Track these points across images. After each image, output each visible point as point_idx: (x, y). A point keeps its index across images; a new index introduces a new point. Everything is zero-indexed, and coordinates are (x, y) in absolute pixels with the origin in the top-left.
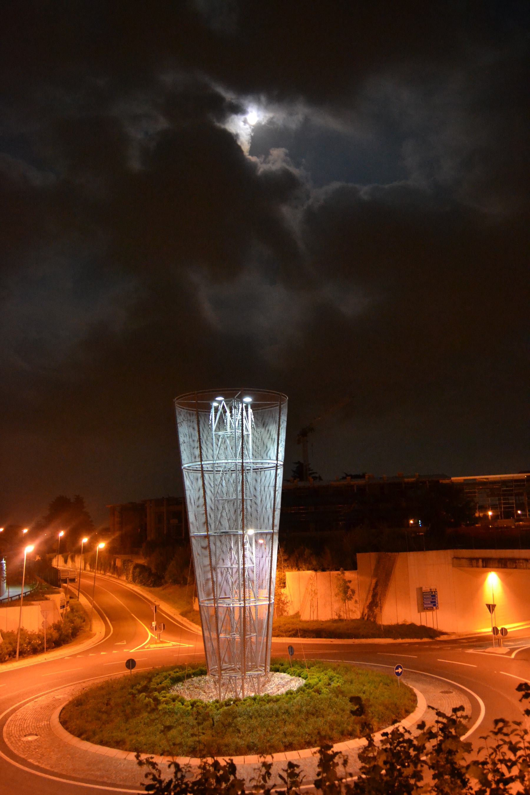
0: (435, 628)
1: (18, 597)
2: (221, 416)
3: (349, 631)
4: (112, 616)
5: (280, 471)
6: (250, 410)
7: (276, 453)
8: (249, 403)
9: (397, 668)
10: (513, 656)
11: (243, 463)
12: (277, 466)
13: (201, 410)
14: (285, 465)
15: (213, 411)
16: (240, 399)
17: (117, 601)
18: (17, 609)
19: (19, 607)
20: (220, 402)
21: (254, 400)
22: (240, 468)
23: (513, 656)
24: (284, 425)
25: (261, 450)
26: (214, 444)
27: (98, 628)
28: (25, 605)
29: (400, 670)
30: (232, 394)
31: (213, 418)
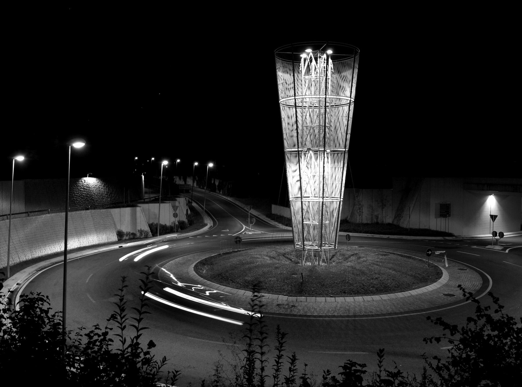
0: (447, 231)
1: (62, 258)
2: (308, 66)
3: (282, 311)
4: (215, 215)
5: (352, 107)
6: (330, 61)
7: (348, 93)
8: (330, 55)
9: (428, 251)
10: (507, 251)
11: (326, 98)
12: (350, 102)
13: (293, 61)
14: (355, 102)
15: (302, 60)
16: (324, 51)
17: (218, 206)
18: (157, 205)
19: (158, 204)
20: (308, 54)
21: (335, 51)
22: (323, 104)
23: (507, 251)
24: (356, 71)
25: (338, 89)
26: (303, 85)
27: (209, 223)
28: (162, 202)
29: (430, 252)
30: (319, 48)
31: (303, 66)
